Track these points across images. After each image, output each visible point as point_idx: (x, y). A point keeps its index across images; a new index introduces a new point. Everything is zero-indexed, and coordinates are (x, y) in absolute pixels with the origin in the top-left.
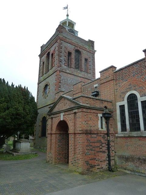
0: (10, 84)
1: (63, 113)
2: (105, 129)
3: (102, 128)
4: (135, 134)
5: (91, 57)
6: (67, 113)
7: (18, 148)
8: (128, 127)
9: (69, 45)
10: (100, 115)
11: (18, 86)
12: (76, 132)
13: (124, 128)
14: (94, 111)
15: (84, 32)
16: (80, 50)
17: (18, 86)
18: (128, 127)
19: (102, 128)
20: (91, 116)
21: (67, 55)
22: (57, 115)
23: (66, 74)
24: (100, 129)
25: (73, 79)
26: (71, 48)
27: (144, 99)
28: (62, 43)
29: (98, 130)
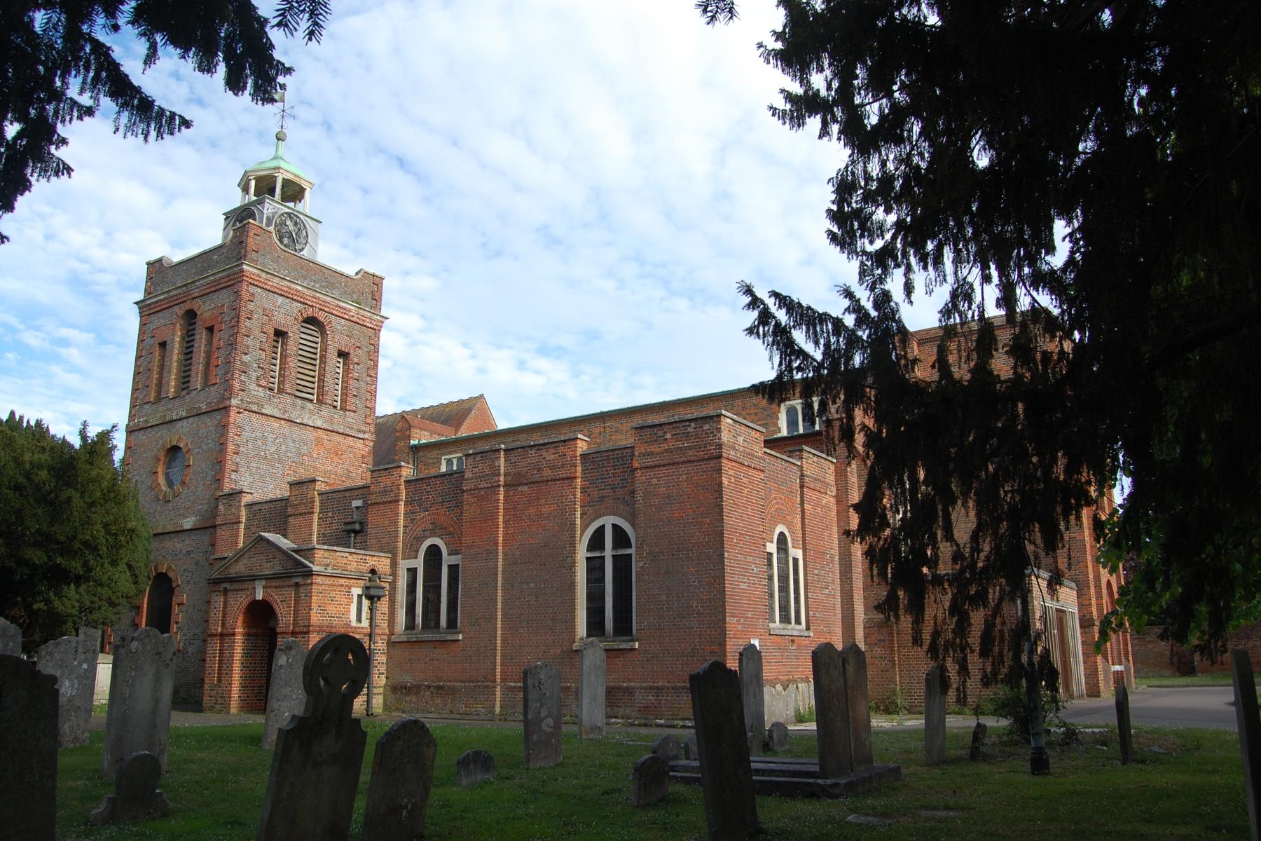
1: (264, 582)
2: (365, 623)
3: (359, 620)
4: (428, 636)
5: (365, 341)
6: (278, 583)
7: (1138, 631)
8: (419, 620)
9: (280, 299)
10: (357, 591)
11: (33, 423)
12: (297, 630)
13: (596, 624)
14: (342, 581)
16: (321, 316)
17: (33, 423)
18: (419, 620)
19: (359, 620)
21: (267, 339)
23: (261, 419)
24: (354, 623)
25: (285, 437)
26: (286, 314)
27: (455, 560)
28: (253, 295)
29: (348, 625)
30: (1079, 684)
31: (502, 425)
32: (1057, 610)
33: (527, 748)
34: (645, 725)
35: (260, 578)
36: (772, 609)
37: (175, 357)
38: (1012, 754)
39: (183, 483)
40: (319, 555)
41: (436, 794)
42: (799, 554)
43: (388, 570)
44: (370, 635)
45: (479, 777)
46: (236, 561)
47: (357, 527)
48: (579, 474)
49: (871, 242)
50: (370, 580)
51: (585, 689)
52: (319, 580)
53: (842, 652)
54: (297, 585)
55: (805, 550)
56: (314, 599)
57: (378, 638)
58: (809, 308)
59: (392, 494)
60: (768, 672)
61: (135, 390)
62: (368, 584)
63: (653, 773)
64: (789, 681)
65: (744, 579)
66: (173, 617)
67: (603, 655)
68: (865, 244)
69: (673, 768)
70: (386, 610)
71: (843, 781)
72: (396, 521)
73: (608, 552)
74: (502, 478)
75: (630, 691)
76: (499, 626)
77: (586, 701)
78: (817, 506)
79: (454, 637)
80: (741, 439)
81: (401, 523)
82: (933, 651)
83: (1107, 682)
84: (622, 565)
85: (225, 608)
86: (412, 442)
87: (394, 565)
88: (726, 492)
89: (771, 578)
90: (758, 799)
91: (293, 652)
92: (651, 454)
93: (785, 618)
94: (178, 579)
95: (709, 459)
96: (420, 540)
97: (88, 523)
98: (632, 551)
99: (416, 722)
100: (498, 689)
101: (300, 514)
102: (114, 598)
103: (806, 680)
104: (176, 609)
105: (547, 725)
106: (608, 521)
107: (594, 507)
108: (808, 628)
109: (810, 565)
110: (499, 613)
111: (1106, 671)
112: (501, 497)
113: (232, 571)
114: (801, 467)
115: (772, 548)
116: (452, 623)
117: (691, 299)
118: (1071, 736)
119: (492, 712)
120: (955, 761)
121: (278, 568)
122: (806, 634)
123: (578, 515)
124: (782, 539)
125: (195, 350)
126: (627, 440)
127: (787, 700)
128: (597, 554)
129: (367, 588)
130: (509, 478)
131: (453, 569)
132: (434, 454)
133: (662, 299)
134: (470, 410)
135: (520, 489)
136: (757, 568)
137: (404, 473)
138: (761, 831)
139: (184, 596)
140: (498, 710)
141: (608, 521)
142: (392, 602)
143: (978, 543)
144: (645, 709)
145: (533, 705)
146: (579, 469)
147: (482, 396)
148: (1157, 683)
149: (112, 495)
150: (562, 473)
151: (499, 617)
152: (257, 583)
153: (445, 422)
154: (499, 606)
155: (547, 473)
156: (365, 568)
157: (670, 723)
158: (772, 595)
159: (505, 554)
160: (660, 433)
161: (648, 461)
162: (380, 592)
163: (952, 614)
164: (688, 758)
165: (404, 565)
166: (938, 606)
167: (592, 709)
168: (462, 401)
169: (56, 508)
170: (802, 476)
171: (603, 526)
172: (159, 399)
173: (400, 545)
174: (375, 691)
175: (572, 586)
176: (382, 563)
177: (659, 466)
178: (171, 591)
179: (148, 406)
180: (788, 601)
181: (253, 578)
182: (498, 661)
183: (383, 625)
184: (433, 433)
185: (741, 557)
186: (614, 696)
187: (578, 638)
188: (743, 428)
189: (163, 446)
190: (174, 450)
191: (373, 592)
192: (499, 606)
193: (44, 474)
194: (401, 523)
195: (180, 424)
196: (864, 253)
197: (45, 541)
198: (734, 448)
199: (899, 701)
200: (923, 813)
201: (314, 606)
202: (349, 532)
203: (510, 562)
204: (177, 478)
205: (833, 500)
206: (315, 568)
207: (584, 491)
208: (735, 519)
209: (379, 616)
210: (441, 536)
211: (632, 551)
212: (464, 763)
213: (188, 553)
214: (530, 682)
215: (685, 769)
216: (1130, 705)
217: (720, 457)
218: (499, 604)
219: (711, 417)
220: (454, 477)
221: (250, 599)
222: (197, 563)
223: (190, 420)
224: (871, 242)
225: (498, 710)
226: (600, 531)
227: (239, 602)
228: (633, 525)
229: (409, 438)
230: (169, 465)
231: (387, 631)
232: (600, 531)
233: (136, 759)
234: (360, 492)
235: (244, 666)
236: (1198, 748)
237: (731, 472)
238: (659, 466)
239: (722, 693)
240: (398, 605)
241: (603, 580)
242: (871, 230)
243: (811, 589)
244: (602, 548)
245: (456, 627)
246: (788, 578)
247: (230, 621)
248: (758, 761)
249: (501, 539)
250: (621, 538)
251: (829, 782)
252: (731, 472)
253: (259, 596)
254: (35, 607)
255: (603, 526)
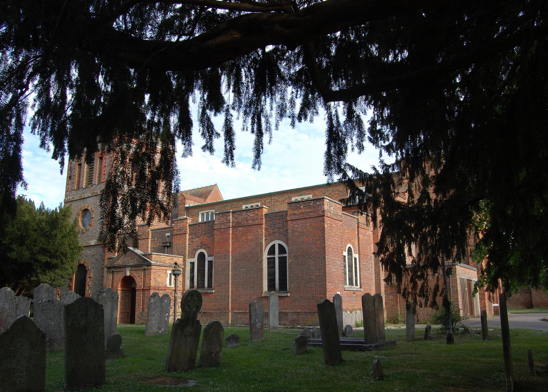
0: (37, 206)
1: (130, 268)
3: (170, 284)
6: (134, 269)
8: (196, 284)
10: (169, 272)
12: (145, 288)
13: (271, 286)
14: (163, 268)
15: (202, 150)
18: (196, 284)
19: (170, 284)
20: (160, 273)
22: (122, 270)
24: (168, 286)
27: (211, 259)
29: (166, 286)
30: (477, 312)
31: (225, 199)
32: (467, 280)
33: (251, 334)
34: (293, 328)
35: (128, 266)
36: (345, 279)
37: (85, 170)
38: (441, 337)
39: (90, 225)
40: (154, 257)
41: (224, 350)
42: (357, 256)
43: (182, 263)
44: (175, 291)
45: (234, 345)
46: (118, 259)
47: (168, 244)
48: (264, 223)
49: (384, 142)
50: (175, 267)
51: (271, 312)
52: (154, 267)
53: (374, 296)
54: (144, 269)
55: (359, 254)
56: (152, 276)
57: (178, 292)
58: (360, 171)
59: (183, 231)
60: (344, 306)
61: (68, 184)
62: (174, 269)
63: (302, 342)
64: (353, 309)
65: (334, 267)
66: (87, 283)
67: (278, 298)
68: (381, 143)
69: (309, 341)
70: (181, 280)
71: (373, 345)
72: (185, 242)
73: (277, 256)
74: (231, 224)
75: (286, 314)
76: (230, 287)
77: (271, 316)
78: (365, 235)
79: (211, 291)
80: (332, 208)
81: (187, 243)
82: (404, 295)
83: (490, 310)
84: (283, 261)
85: (113, 279)
86: (186, 206)
87: (184, 261)
88: (326, 230)
89: (345, 266)
90: (342, 352)
91: (156, 297)
92: (294, 214)
93: (351, 283)
94: (89, 267)
95: (319, 217)
96: (196, 250)
97: (63, 244)
98: (287, 255)
99: (217, 322)
100: (230, 313)
101: (143, 239)
102: (63, 275)
103: (360, 309)
104: (88, 280)
105: (258, 325)
106: (277, 242)
107: (271, 236)
108: (361, 288)
109: (361, 261)
110: (230, 281)
111: (490, 306)
112: (231, 232)
113: (116, 263)
114: (358, 219)
115: (345, 253)
116: (210, 286)
117: (309, 134)
118: (466, 331)
119: (228, 323)
120: (418, 340)
121: (136, 262)
122: (360, 290)
123: (264, 240)
124: (350, 250)
125: (95, 167)
126: (284, 207)
127: (352, 317)
128: (272, 256)
129: (174, 271)
130: (234, 224)
131: (210, 263)
132: (196, 211)
133: (296, 135)
134: (211, 191)
135: (239, 229)
136: (339, 262)
137: (188, 222)
138: (343, 361)
139: (91, 274)
140: (230, 322)
141: (277, 242)
142: (184, 276)
143: (420, 257)
144: (293, 322)
145: (253, 318)
146: (264, 220)
147: (216, 184)
148: (515, 311)
149: (72, 233)
150: (257, 222)
151: (230, 283)
152: (127, 268)
153: (200, 196)
154: (230, 278)
155: (250, 222)
156: (173, 262)
157: (303, 327)
158: (345, 274)
159: (232, 256)
160: (298, 206)
161: (293, 217)
162: (179, 272)
163: (411, 281)
164: (313, 338)
165: (189, 261)
166: (406, 280)
167: (273, 321)
168: (207, 187)
169: (48, 237)
170: (358, 223)
171: (274, 245)
172: (78, 188)
173: (187, 252)
174: (177, 314)
175: (261, 270)
176: (180, 260)
177: (298, 219)
178: (86, 272)
179: (74, 192)
180: (352, 276)
181: (125, 267)
182: (230, 301)
183: (180, 287)
184: (195, 201)
185: (332, 258)
186: (282, 315)
187: (264, 292)
188: (333, 203)
189: (81, 209)
190: (86, 211)
191: (176, 272)
192: (230, 278)
193: (44, 224)
194: (187, 243)
195: (88, 199)
196: (382, 146)
197: (44, 251)
198: (330, 212)
199: (399, 319)
200: (403, 355)
201: (152, 278)
202: (164, 247)
203: (235, 260)
204: (87, 223)
205: (371, 233)
206: (152, 262)
207: (266, 230)
208: (330, 242)
209: (178, 283)
210: (205, 249)
211: (287, 255)
212: (228, 339)
213: (93, 255)
214: (252, 309)
215: (313, 341)
216: (488, 320)
217: (324, 216)
218: (230, 277)
219: (320, 199)
220: (209, 224)
221: (124, 276)
222: (97, 260)
223: (93, 198)
224: (384, 142)
225: (230, 322)
226: (273, 247)
227: (119, 277)
228: (287, 244)
229: (185, 204)
230: (83, 217)
231: (182, 289)
232: (273, 247)
233: (114, 336)
234: (169, 229)
235: (121, 304)
236: (517, 335)
237: (328, 222)
238: (298, 219)
239: (329, 311)
240: (186, 278)
241: (274, 267)
242: (384, 138)
243: (362, 271)
244: (274, 254)
245: (211, 287)
246: (352, 266)
247: (115, 285)
248: (341, 339)
249: (231, 250)
250: (282, 250)
251: (368, 345)
252: (328, 222)
253: (128, 274)
254: (32, 279)
255: (274, 245)
